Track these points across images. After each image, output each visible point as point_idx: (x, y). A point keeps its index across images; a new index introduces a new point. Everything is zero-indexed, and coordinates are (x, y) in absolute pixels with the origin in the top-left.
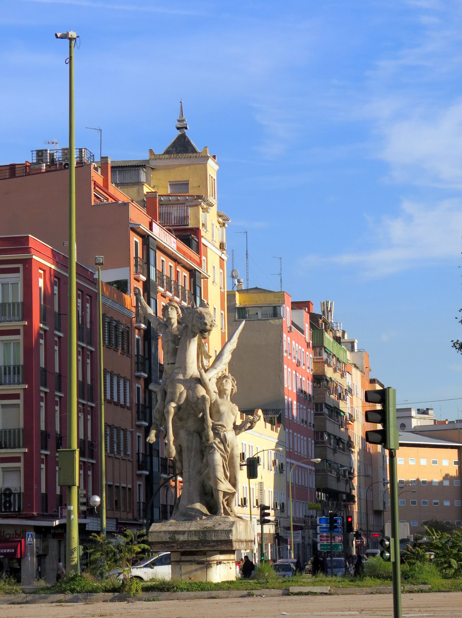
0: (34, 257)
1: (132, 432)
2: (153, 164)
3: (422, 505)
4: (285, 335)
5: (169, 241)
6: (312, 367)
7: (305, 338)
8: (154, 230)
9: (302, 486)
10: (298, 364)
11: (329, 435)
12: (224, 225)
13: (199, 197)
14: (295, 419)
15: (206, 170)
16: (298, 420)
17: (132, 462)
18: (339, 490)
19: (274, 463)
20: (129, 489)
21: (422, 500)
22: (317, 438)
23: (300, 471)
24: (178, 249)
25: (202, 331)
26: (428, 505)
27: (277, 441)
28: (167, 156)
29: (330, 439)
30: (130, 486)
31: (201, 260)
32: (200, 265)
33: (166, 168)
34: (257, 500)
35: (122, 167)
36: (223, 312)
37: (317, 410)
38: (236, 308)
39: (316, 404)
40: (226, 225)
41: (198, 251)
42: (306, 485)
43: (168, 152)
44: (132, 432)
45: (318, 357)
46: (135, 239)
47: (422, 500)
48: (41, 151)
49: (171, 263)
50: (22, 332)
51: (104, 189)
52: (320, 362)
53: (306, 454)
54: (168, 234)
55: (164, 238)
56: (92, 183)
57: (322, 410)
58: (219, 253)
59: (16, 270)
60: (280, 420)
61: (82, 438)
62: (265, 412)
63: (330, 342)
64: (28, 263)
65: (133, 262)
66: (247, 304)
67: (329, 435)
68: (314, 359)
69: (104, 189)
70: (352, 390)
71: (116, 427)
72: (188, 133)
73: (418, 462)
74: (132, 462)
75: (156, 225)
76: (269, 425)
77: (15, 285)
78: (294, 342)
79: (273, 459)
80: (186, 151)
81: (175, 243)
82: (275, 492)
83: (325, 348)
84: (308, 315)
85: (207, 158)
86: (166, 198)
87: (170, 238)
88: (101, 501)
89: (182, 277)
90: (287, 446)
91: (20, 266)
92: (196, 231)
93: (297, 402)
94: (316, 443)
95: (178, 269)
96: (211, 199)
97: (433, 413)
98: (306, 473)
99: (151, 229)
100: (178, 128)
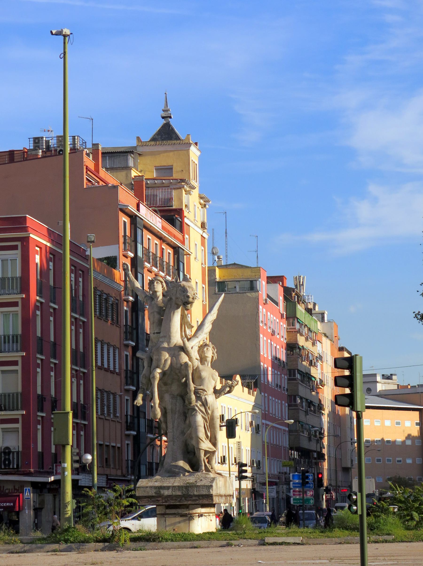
0: (31, 235)
1: (120, 396)
2: (140, 150)
3: (387, 463)
4: (261, 307)
5: (155, 221)
6: (285, 336)
7: (279, 310)
8: (141, 210)
9: (276, 445)
10: (273, 334)
11: (301, 398)
12: (205, 206)
13: (183, 180)
14: (270, 383)
15: (189, 156)
16: (273, 385)
17: (121, 423)
18: (311, 449)
19: (251, 424)
20: (118, 448)
21: (387, 458)
22: (291, 401)
23: (275, 432)
24: (163, 228)
25: (185, 303)
26: (391, 463)
27: (253, 404)
28: (153, 143)
29: (302, 402)
30: (119, 445)
31: (184, 238)
32: (183, 242)
33: (152, 154)
34: (235, 458)
35: (112, 153)
36: (204, 286)
37: (290, 375)
38: (216, 282)
39: (290, 370)
40: (207, 206)
41: (181, 230)
42: (281, 444)
43: (154, 139)
44: (120, 396)
45: (291, 327)
46: (124, 219)
47: (387, 458)
48: (38, 138)
49: (157, 241)
50: (20, 304)
51: (95, 173)
52: (293, 331)
53: (280, 415)
54: (154, 214)
55: (150, 218)
56: (85, 167)
57: (294, 375)
58: (201, 231)
59: (15, 248)
60: (256, 385)
61: (76, 401)
62: (243, 377)
63: (302, 313)
64: (25, 240)
65: (121, 240)
66: (226, 278)
67: (301, 398)
68: (287, 329)
69: (95, 173)
70: (322, 357)
71: (106, 391)
72: (172, 122)
73: (383, 423)
74: (121, 423)
75: (143, 206)
76: (246, 390)
77: (13, 261)
78: (269, 314)
79: (250, 420)
80: (171, 139)
81: (160, 223)
82: (251, 451)
83: (297, 318)
84: (282, 289)
85: (190, 145)
86: (152, 181)
87: (156, 218)
88: (93, 459)
89: (166, 254)
90: (263, 408)
91: (19, 244)
92: (180, 212)
93: (272, 368)
94: (289, 406)
95: (163, 247)
96: (193, 182)
97: (396, 379)
98: (280, 434)
99: (138, 210)
100: (163, 118)
